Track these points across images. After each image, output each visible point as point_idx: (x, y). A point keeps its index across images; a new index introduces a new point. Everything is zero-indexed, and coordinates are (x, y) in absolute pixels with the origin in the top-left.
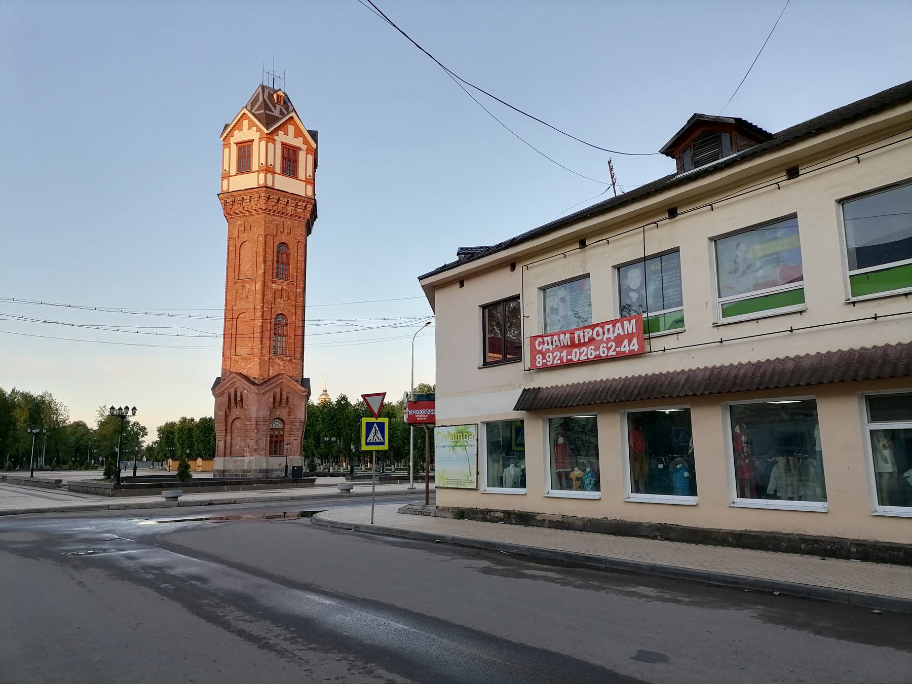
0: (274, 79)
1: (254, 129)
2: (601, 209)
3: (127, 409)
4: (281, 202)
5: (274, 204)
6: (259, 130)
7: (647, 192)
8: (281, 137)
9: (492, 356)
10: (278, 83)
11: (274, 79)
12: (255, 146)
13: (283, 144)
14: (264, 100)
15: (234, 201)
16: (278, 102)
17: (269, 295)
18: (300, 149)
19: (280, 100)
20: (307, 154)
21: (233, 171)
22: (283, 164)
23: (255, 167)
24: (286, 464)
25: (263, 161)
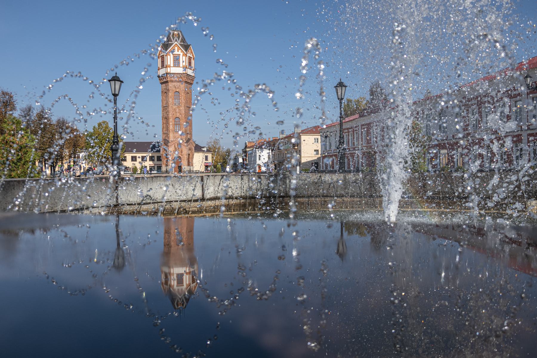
1: (180, 51)
21: (172, 65)
23: (181, 65)
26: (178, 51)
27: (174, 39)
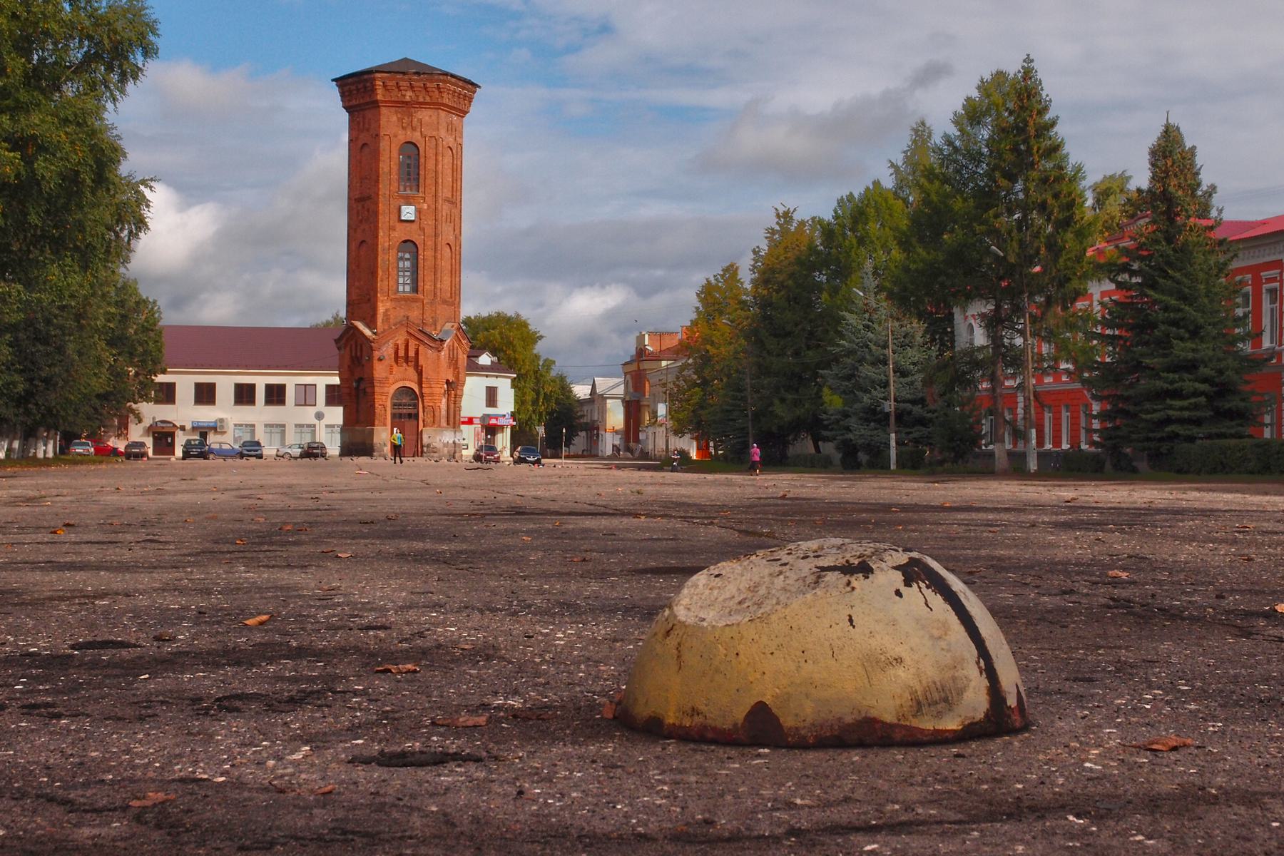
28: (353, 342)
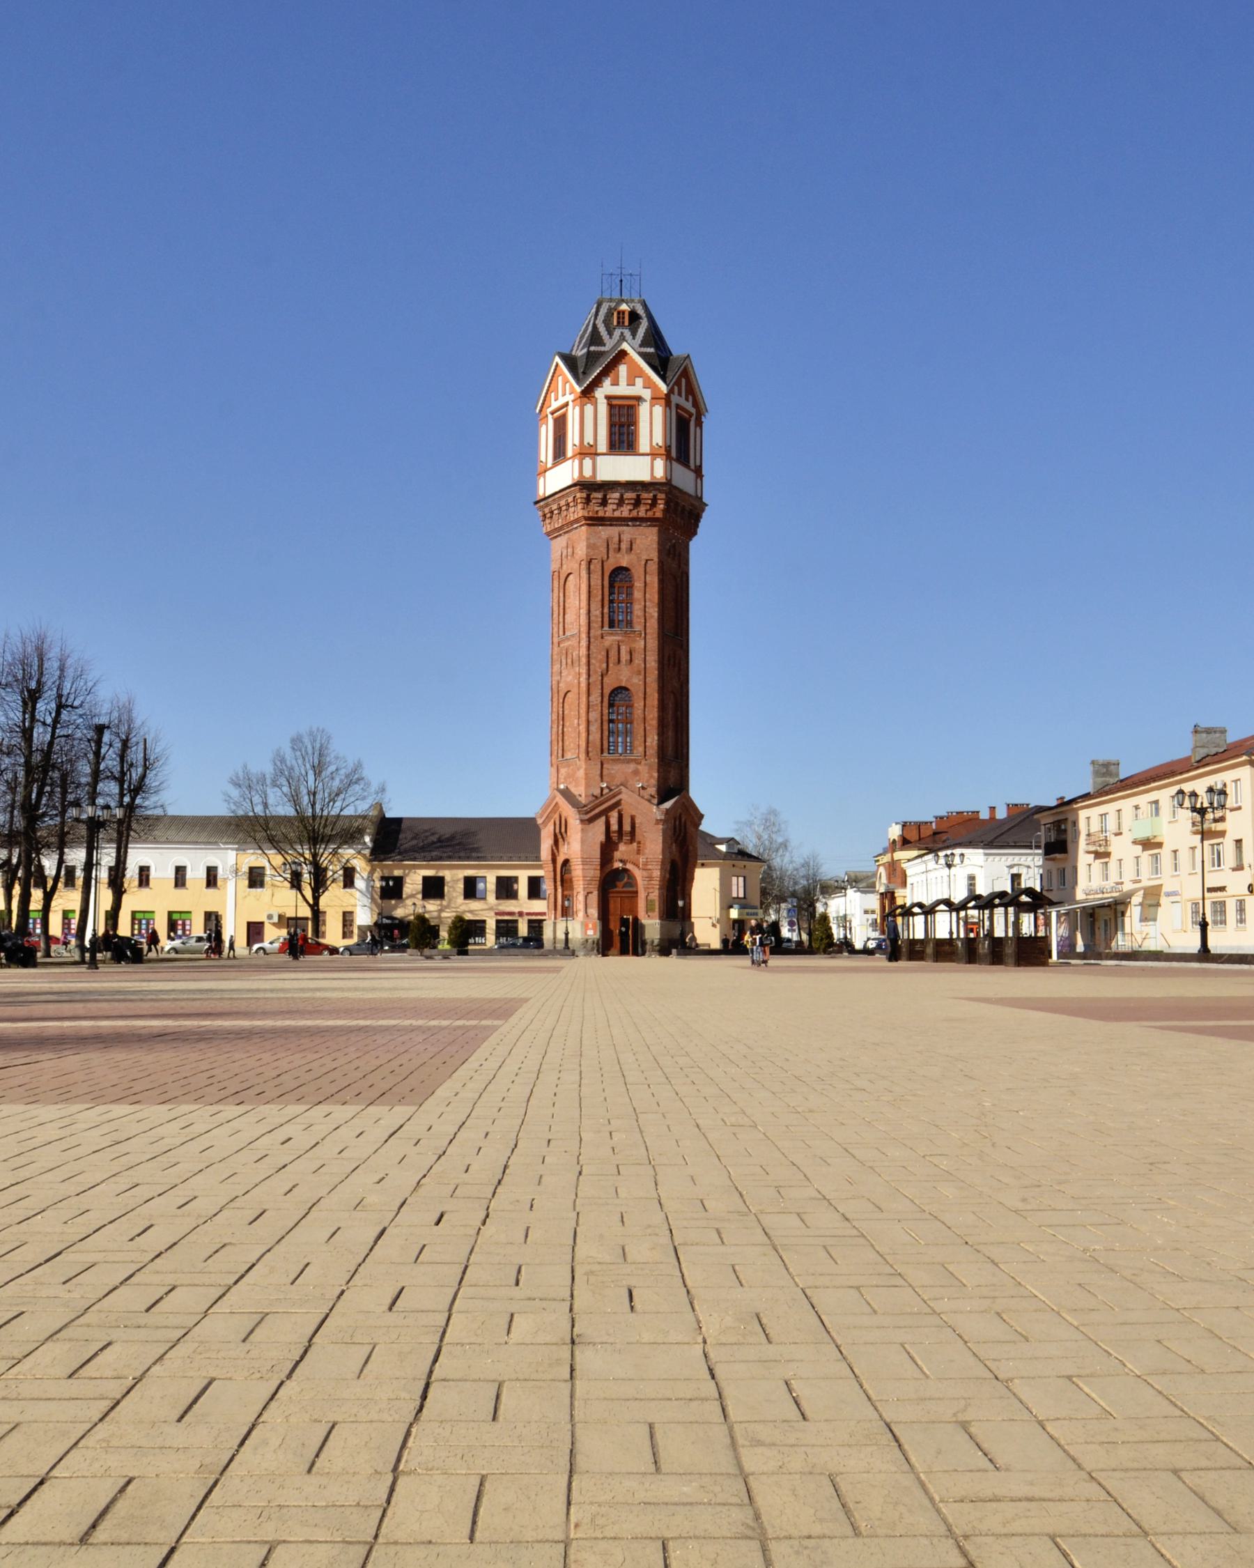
0: (621, 281)
1: (639, 381)
2: (1136, 779)
3: (1222, 796)
4: (594, 501)
5: (648, 507)
6: (648, 384)
7: (1171, 768)
8: (606, 388)
9: (67, 1024)
10: (628, 286)
11: (621, 281)
12: (644, 409)
13: (608, 398)
14: (595, 326)
15: (560, 508)
16: (618, 322)
17: (598, 657)
18: (639, 399)
19: (623, 318)
20: (652, 406)
21: (603, 446)
22: (611, 434)
24: (567, 930)
25: (577, 443)
26: (631, 383)
27: (610, 334)
28: (557, 816)
